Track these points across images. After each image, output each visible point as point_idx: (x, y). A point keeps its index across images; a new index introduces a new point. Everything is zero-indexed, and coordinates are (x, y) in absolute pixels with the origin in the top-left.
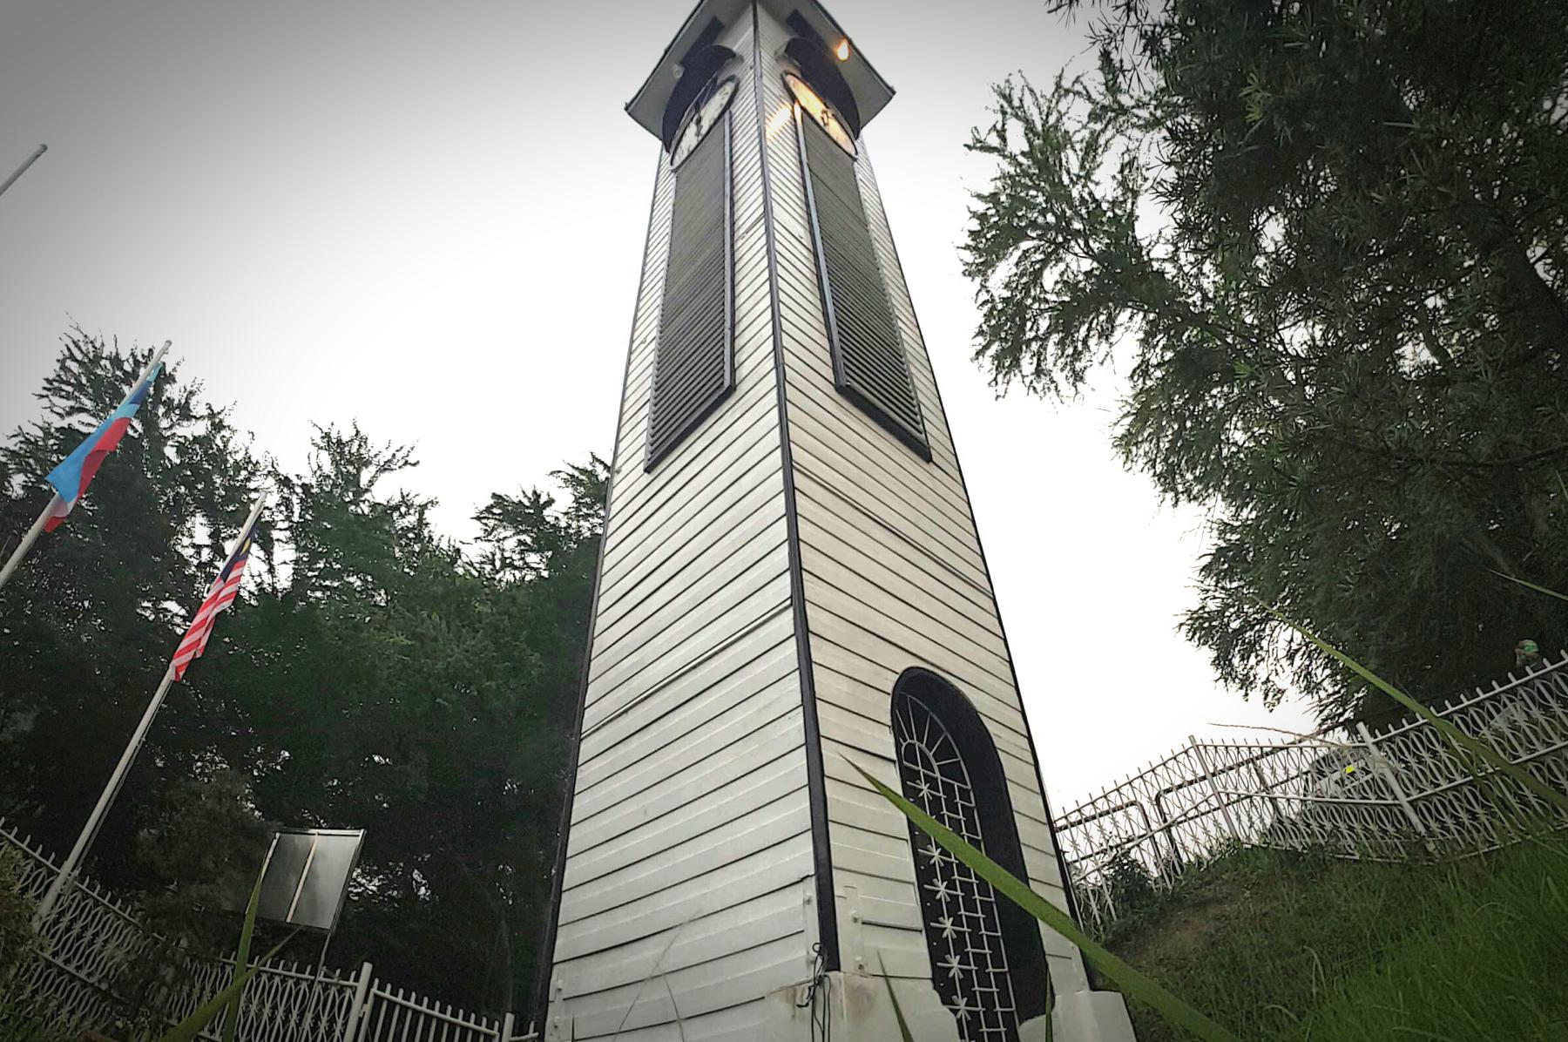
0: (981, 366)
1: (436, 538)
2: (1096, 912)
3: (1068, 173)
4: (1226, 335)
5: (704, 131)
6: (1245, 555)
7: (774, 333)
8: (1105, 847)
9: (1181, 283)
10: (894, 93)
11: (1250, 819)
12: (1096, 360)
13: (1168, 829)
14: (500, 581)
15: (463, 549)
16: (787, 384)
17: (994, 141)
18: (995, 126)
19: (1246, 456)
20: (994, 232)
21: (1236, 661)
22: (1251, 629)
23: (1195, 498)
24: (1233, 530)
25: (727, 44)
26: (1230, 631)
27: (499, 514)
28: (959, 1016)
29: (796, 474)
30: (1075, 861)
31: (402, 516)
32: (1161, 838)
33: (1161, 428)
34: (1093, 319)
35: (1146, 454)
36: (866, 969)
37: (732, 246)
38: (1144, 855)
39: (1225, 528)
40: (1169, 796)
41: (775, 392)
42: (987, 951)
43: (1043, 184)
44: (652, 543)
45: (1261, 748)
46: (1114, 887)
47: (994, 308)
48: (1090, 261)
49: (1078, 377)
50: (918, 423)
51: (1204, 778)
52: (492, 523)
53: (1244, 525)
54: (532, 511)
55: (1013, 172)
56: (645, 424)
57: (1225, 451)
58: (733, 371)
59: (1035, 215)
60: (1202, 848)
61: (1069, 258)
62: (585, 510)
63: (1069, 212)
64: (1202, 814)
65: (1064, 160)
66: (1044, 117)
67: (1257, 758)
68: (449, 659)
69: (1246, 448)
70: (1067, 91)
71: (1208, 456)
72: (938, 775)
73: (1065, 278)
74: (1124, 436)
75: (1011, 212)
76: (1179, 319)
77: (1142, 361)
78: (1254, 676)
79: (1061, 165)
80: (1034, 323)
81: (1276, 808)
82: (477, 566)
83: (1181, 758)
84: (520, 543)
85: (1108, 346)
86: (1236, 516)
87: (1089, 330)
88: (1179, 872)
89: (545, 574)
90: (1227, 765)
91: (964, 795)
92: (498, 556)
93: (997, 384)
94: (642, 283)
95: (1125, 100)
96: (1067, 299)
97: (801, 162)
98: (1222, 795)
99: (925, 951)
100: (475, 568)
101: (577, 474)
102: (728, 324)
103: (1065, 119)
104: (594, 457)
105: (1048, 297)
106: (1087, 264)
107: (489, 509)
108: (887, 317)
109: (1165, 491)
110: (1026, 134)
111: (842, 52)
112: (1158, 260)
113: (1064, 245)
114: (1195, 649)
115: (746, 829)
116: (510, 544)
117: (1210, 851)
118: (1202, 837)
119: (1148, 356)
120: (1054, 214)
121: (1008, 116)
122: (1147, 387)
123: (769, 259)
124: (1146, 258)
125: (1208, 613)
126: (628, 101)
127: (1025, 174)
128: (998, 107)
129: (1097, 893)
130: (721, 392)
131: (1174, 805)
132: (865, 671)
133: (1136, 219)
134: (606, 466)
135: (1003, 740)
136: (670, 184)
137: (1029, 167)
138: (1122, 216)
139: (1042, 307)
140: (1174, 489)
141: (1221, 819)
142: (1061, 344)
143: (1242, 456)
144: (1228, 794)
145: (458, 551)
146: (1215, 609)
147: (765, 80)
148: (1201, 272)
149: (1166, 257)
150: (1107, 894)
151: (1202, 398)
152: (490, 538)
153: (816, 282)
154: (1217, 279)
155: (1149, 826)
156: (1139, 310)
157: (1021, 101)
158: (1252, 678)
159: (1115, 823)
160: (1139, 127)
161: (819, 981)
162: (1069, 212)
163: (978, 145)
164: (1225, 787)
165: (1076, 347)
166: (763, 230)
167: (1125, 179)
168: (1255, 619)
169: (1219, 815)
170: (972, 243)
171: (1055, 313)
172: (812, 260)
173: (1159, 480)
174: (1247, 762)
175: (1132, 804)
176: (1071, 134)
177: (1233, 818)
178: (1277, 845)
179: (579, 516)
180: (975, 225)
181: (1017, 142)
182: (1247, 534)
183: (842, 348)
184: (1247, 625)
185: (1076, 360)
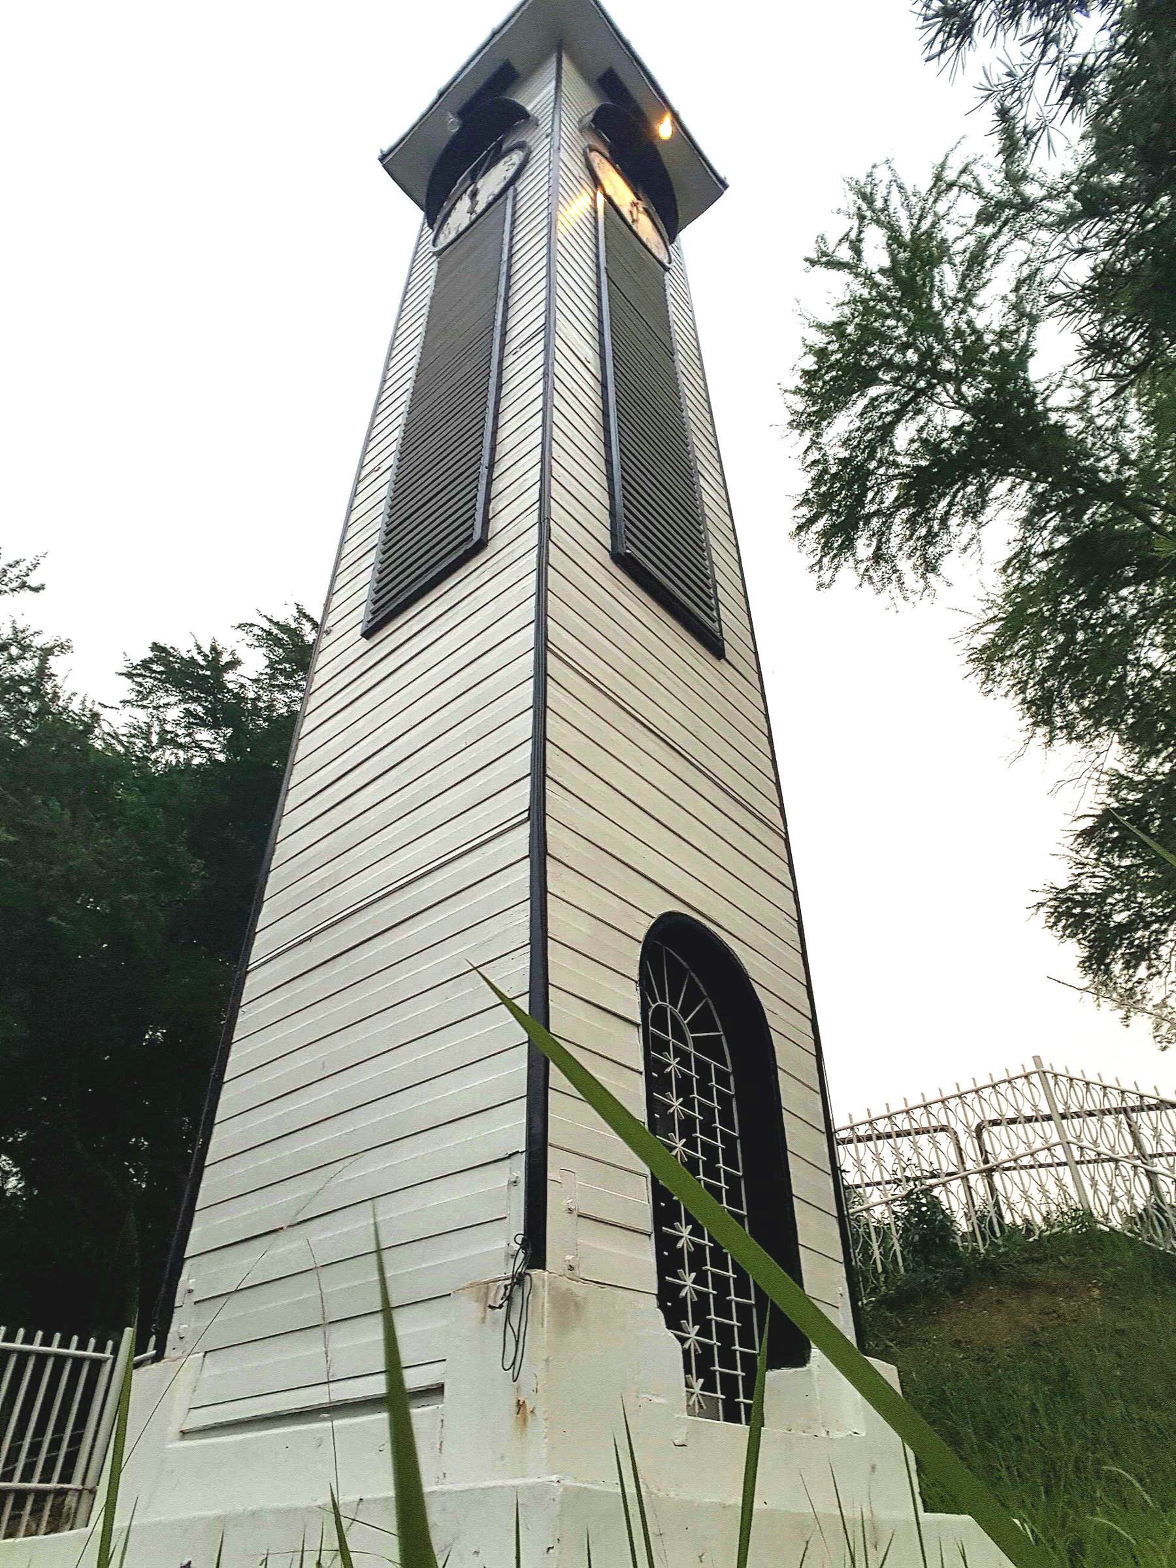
0: (802, 545)
1: (64, 696)
2: (877, 1255)
3: (941, 295)
4: (1153, 513)
5: (479, 209)
6: (1148, 822)
7: (541, 479)
8: (899, 1176)
9: (1090, 440)
10: (726, 186)
11: (1112, 1191)
12: (957, 545)
13: (988, 1173)
14: (156, 762)
15: (105, 714)
16: (551, 544)
17: (844, 254)
18: (847, 234)
19: (1165, 683)
20: (834, 373)
21: (1117, 968)
22: (1147, 926)
23: (1079, 738)
24: (1133, 786)
25: (520, 100)
26: (1112, 924)
27: (161, 673)
28: (686, 1346)
29: (550, 656)
30: (858, 1186)
31: (12, 660)
32: (978, 1184)
33: (1039, 642)
34: (958, 491)
35: (1014, 673)
36: (577, 1271)
37: (501, 362)
38: (953, 1200)
39: (1118, 783)
40: (996, 1129)
41: (535, 552)
42: (739, 1372)
43: (905, 311)
44: (362, 728)
45: (1142, 1097)
46: (905, 1230)
47: (825, 471)
48: (961, 413)
49: (930, 566)
50: (712, 609)
51: (1049, 1118)
52: (149, 683)
53: (1150, 781)
54: (208, 673)
55: (866, 295)
56: (367, 576)
57: (1131, 677)
58: (486, 522)
59: (892, 351)
60: (1033, 1210)
61: (932, 408)
62: (282, 679)
63: (937, 348)
64: (1041, 1166)
65: (937, 278)
66: (915, 222)
67: (1133, 1109)
68: (71, 863)
69: (1165, 673)
70: (951, 186)
71: (1104, 681)
72: (691, 1049)
73: (924, 435)
74: (985, 648)
75: (859, 347)
76: (1081, 491)
77: (1022, 548)
78: (1143, 994)
79: (932, 286)
80: (877, 494)
81: (1155, 1188)
82: (125, 739)
83: (1020, 1083)
84: (188, 712)
85: (974, 526)
86: (1139, 766)
87: (951, 505)
88: (998, 1235)
89: (221, 757)
90: (1086, 1107)
91: (722, 1078)
92: (156, 728)
93: (821, 568)
94: (381, 392)
95: (1032, 191)
96: (924, 463)
97: (598, 266)
98: (1074, 1147)
99: (652, 1260)
100: (120, 742)
101: (275, 631)
102: (485, 461)
103: (943, 223)
104: (300, 611)
105: (899, 459)
106: (956, 417)
107: (145, 664)
108: (687, 474)
109: (1035, 724)
110: (889, 246)
111: (665, 130)
112: (1057, 409)
113: (928, 392)
114: (1056, 941)
115: (447, 1091)
116: (173, 714)
117: (1046, 1219)
118: (1037, 1197)
119: (1030, 541)
120: (917, 350)
121: (866, 221)
122: (1025, 583)
123: (546, 383)
124: (1040, 408)
125: (1082, 895)
126: (386, 149)
127: (882, 297)
128: (853, 210)
129: (883, 1233)
130: (469, 546)
131: (1000, 1143)
132: (611, 909)
133: (1032, 355)
134: (315, 625)
135: (777, 1016)
136: (432, 268)
137: (889, 289)
138: (1012, 352)
139: (890, 472)
140: (1049, 722)
141: (1068, 1179)
142: (912, 521)
143: (1158, 683)
144: (1082, 1148)
145: (95, 716)
146: (1092, 890)
147: (563, 155)
148: (1121, 423)
149: (1070, 405)
150: (895, 1237)
151: (1104, 602)
152: (145, 703)
153: (601, 421)
154: (1145, 433)
155: (963, 1163)
156: (1024, 479)
157: (886, 201)
158: (1139, 997)
159: (916, 1149)
160: (1049, 227)
161: (519, 1280)
162: (937, 348)
163: (824, 259)
164: (1078, 1137)
165: (931, 527)
166: (540, 347)
167: (1021, 299)
168: (1152, 914)
169: (1065, 1173)
170: (804, 386)
171: (907, 481)
172: (599, 391)
173: (1029, 709)
174: (1117, 1111)
175: (943, 1129)
176: (950, 242)
177: (1087, 1183)
178: (1152, 1240)
179: (274, 686)
180: (810, 363)
181: (876, 256)
182: (1153, 795)
183: (625, 506)
184: (1139, 920)
185: (930, 543)
